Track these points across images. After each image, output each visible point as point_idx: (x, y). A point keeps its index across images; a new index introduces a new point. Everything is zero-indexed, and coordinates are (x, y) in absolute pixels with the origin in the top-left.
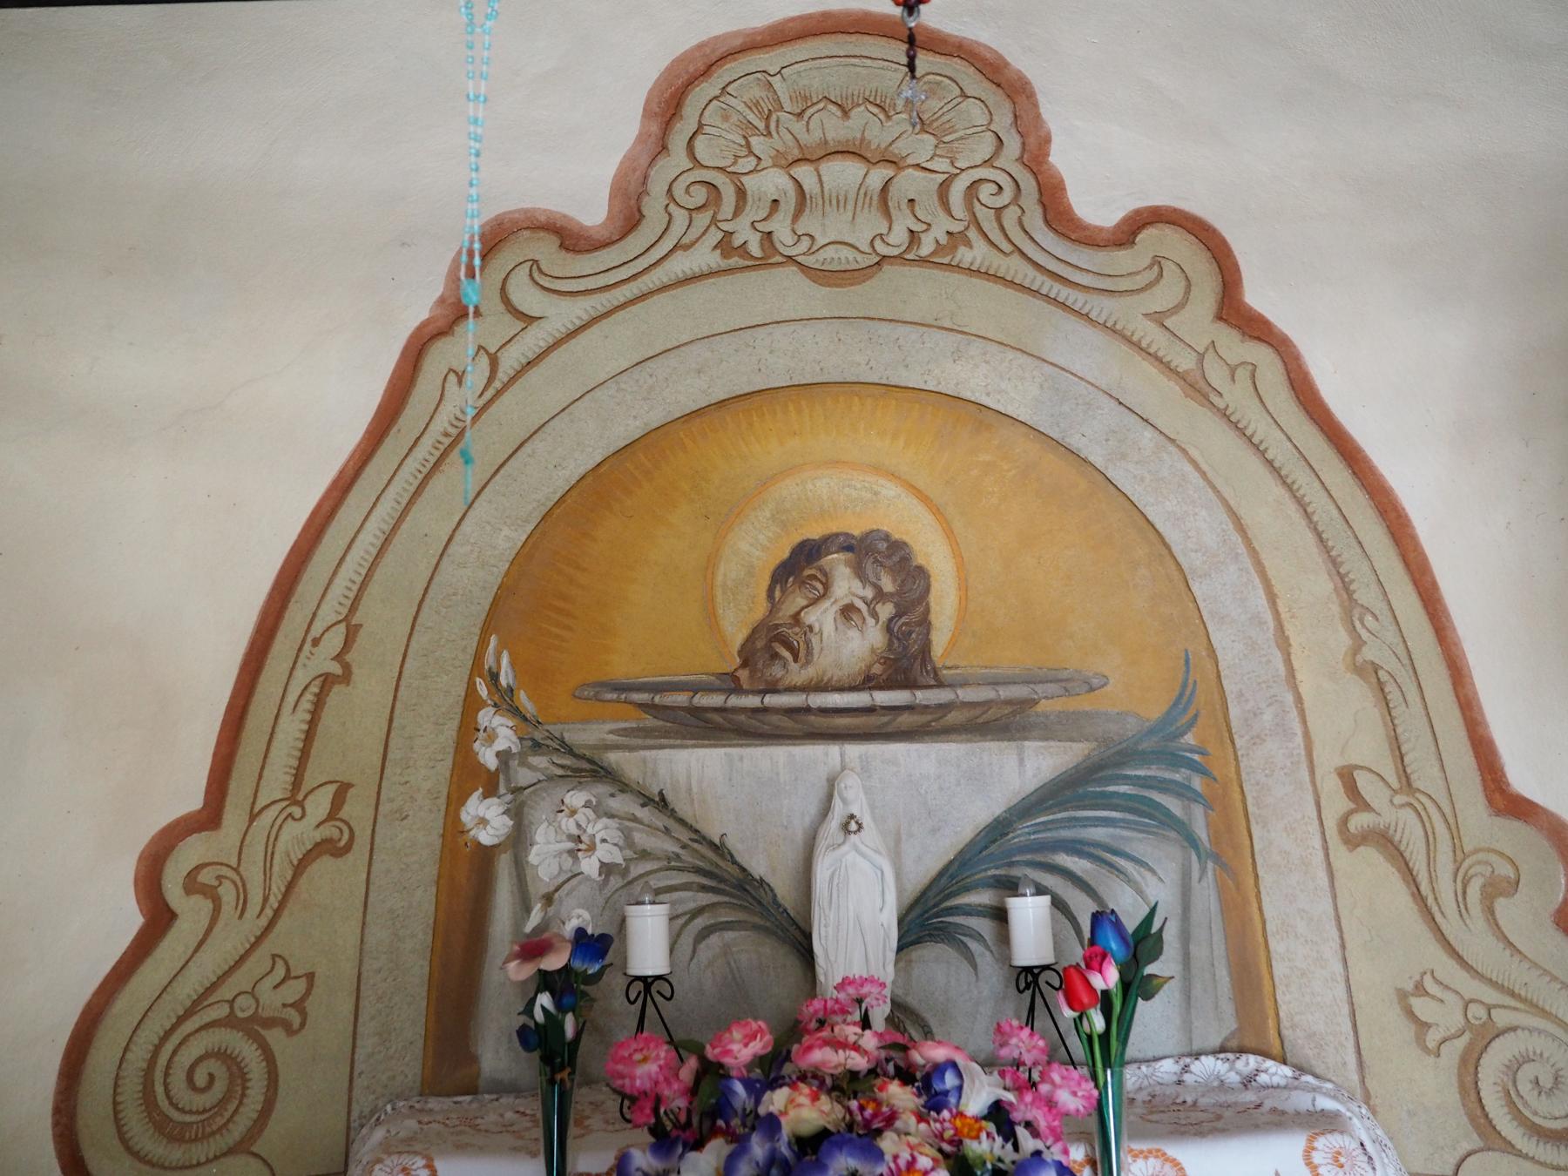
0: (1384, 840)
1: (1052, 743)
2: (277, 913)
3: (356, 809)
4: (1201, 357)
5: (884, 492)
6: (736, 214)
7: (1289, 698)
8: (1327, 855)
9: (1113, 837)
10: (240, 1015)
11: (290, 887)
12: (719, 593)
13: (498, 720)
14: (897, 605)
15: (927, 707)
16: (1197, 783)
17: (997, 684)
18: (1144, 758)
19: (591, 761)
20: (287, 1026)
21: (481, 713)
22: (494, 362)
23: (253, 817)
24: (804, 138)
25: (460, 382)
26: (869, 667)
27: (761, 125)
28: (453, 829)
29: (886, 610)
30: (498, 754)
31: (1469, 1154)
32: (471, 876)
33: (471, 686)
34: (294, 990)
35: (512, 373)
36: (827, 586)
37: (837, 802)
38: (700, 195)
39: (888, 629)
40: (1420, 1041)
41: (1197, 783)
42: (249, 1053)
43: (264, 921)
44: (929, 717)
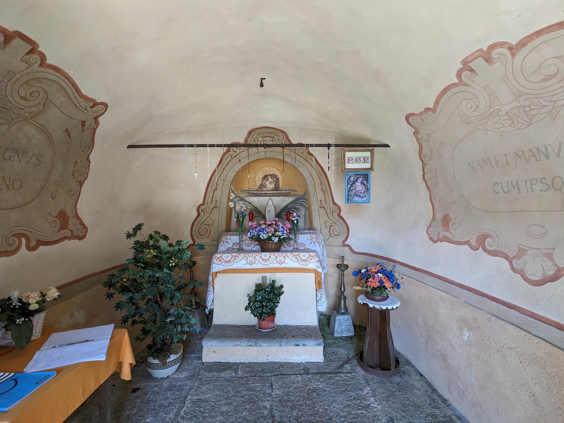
0: (324, 207)
28: (228, 206)
32: (230, 211)
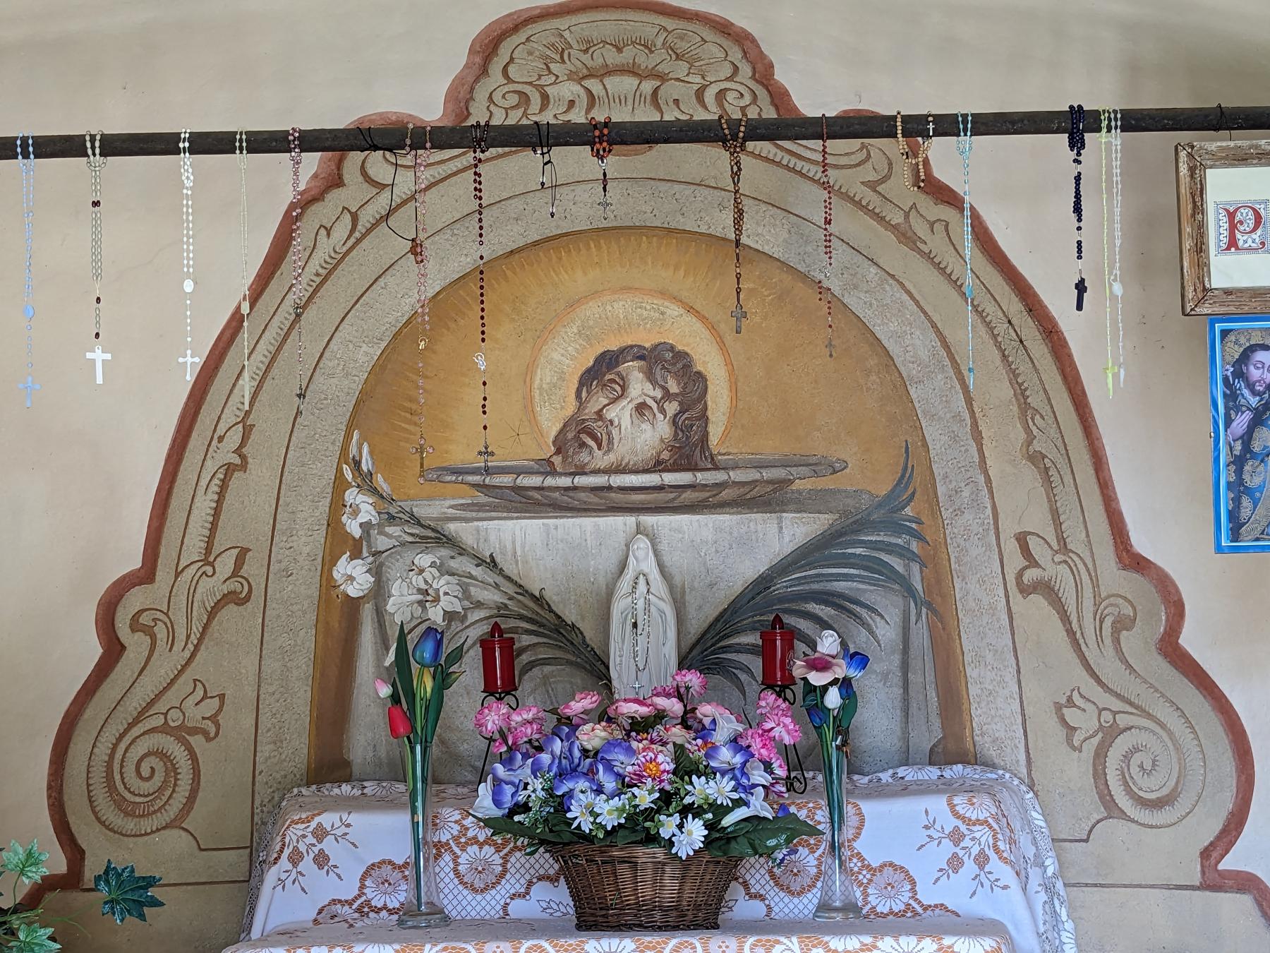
0: (1046, 589)
1: (805, 515)
2: (197, 647)
3: (253, 568)
4: (907, 215)
5: (669, 312)
6: (541, 110)
7: (982, 478)
8: (1008, 602)
9: (851, 589)
10: (172, 724)
11: (205, 627)
12: (536, 394)
13: (361, 498)
14: (681, 404)
15: (706, 485)
16: (915, 546)
17: (761, 467)
18: (874, 526)
19: (434, 530)
20: (205, 733)
21: (347, 492)
22: (355, 218)
23: (177, 575)
24: (590, 63)
25: (328, 235)
26: (659, 454)
27: (558, 57)
28: (328, 584)
29: (672, 408)
30: (361, 525)
31: (1098, 822)
32: (342, 620)
33: (339, 471)
34: (211, 706)
35: (369, 226)
36: (624, 388)
37: (631, 559)
38: (513, 100)
39: (674, 422)
40: (1069, 740)
41: (915, 546)
42: (179, 753)
43: (187, 654)
44: (708, 494)
